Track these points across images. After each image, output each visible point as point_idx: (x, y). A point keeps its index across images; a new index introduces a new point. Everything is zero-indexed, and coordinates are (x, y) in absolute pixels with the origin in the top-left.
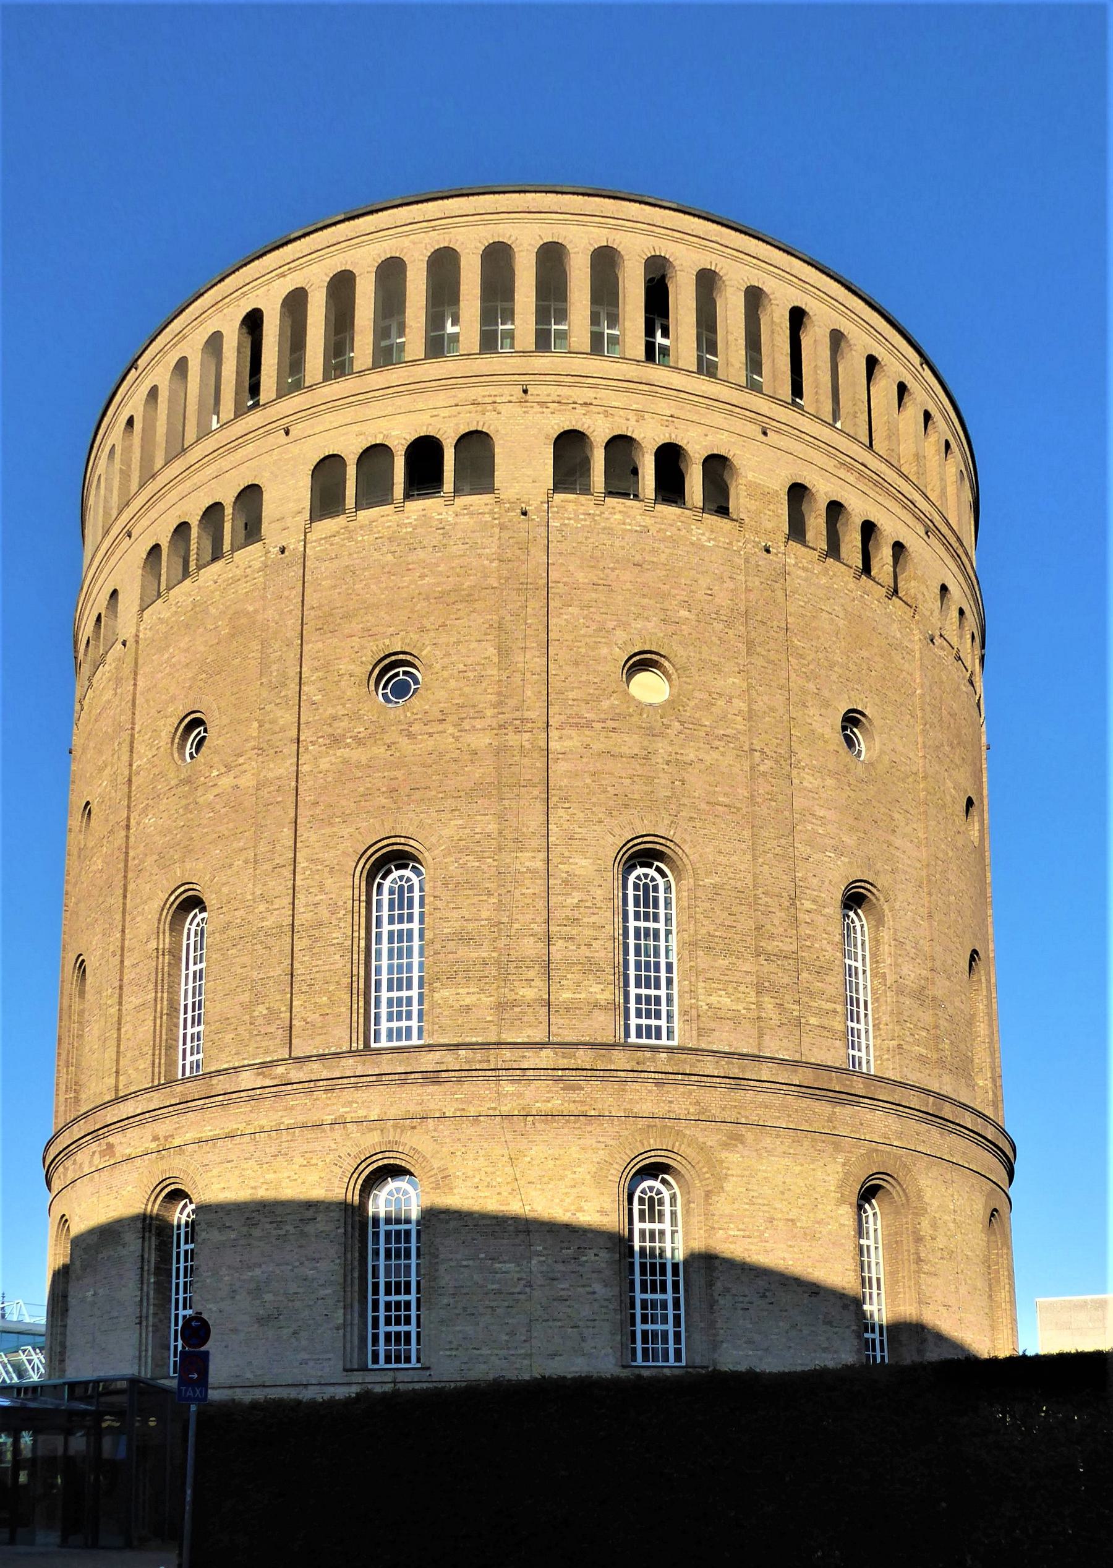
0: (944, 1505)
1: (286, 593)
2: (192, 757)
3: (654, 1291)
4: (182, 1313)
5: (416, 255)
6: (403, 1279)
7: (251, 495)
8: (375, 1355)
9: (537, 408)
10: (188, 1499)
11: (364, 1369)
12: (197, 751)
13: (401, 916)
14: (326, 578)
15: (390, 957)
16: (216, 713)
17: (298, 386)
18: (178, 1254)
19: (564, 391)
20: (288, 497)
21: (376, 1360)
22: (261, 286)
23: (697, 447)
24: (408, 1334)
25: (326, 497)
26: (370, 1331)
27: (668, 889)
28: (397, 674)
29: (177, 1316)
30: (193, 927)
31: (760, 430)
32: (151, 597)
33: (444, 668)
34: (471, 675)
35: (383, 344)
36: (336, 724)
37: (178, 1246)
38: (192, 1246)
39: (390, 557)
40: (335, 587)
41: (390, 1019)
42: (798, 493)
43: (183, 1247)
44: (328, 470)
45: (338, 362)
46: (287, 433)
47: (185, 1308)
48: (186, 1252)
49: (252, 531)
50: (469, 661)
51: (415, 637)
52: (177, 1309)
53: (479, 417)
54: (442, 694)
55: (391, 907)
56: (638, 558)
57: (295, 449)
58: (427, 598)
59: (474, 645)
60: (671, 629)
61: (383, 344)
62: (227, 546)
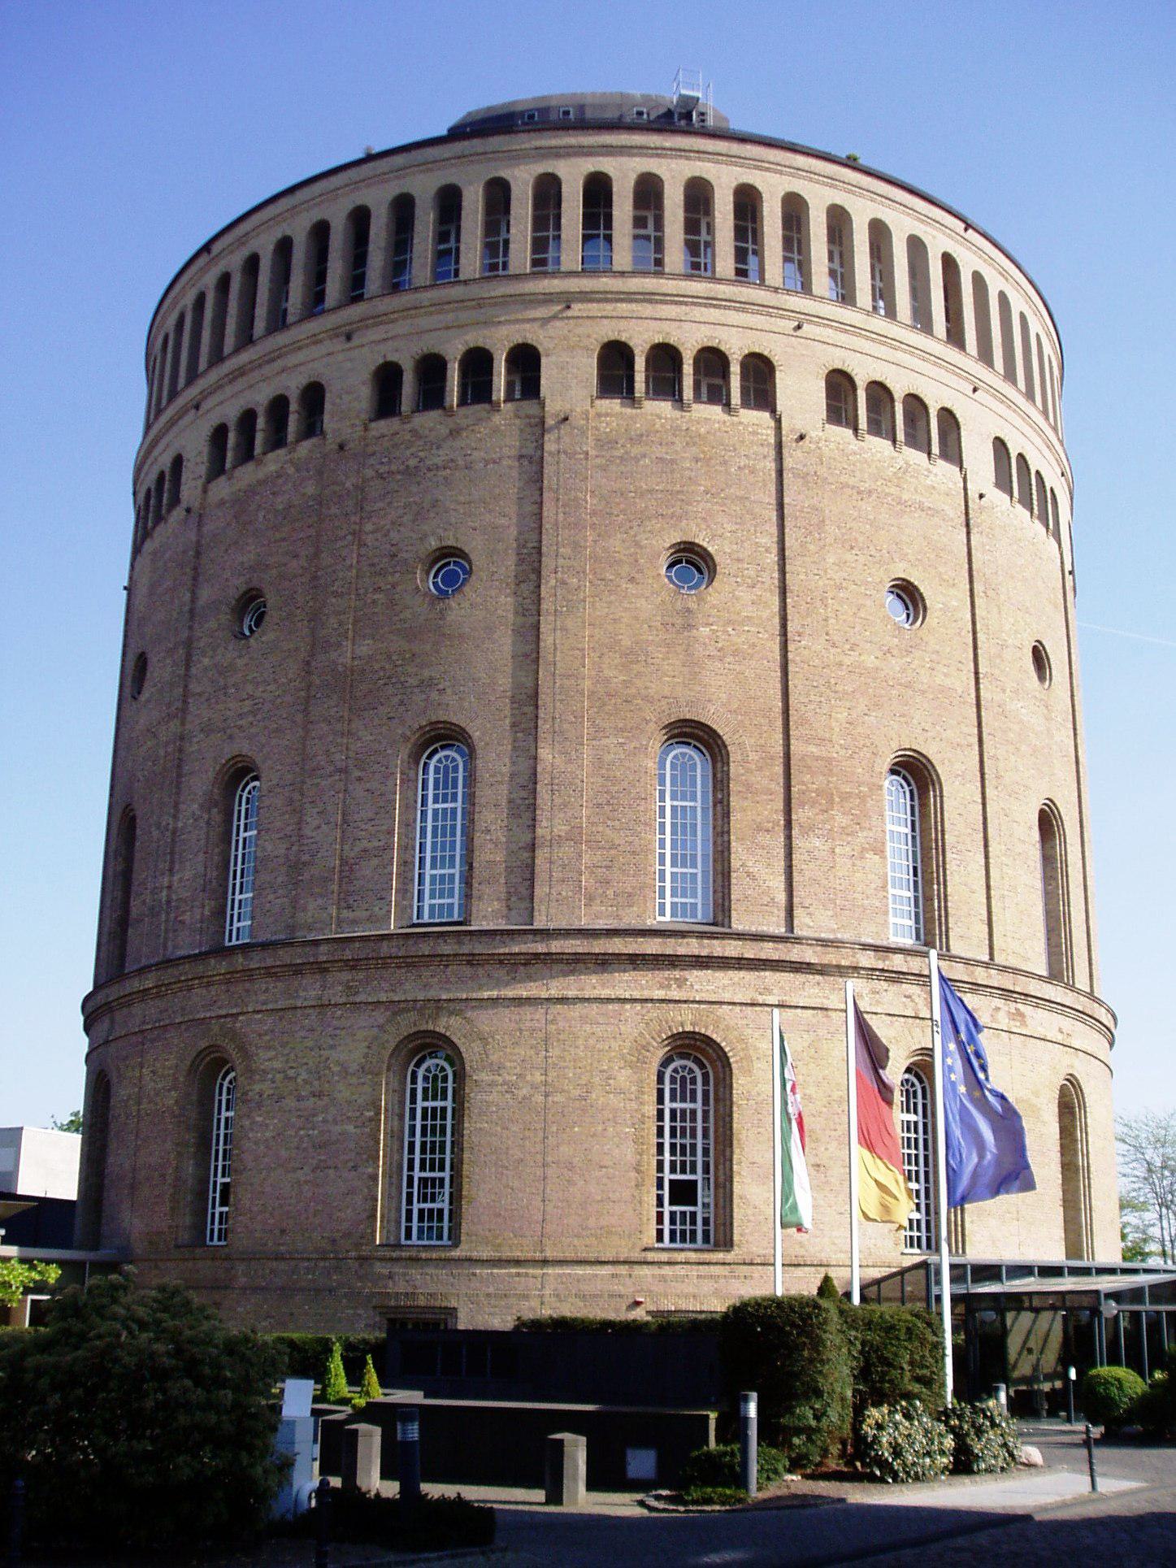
2: (251, 631)
3: (683, 1111)
4: (220, 1180)
6: (438, 1139)
7: (314, 395)
8: (409, 1230)
11: (398, 1246)
12: (257, 625)
13: (445, 796)
15: (424, 1134)
17: (359, 298)
18: (219, 1120)
20: (350, 396)
21: (409, 1236)
23: (736, 347)
24: (442, 1180)
25: (386, 401)
26: (409, 1086)
27: (705, 1076)
28: (448, 564)
29: (215, 1182)
30: (245, 795)
32: (217, 468)
35: (442, 247)
37: (219, 1113)
38: (226, 1209)
41: (432, 897)
43: (224, 1114)
44: (387, 378)
45: (397, 276)
47: (223, 1176)
48: (221, 1213)
49: (312, 426)
52: (216, 1175)
55: (436, 787)
61: (442, 247)
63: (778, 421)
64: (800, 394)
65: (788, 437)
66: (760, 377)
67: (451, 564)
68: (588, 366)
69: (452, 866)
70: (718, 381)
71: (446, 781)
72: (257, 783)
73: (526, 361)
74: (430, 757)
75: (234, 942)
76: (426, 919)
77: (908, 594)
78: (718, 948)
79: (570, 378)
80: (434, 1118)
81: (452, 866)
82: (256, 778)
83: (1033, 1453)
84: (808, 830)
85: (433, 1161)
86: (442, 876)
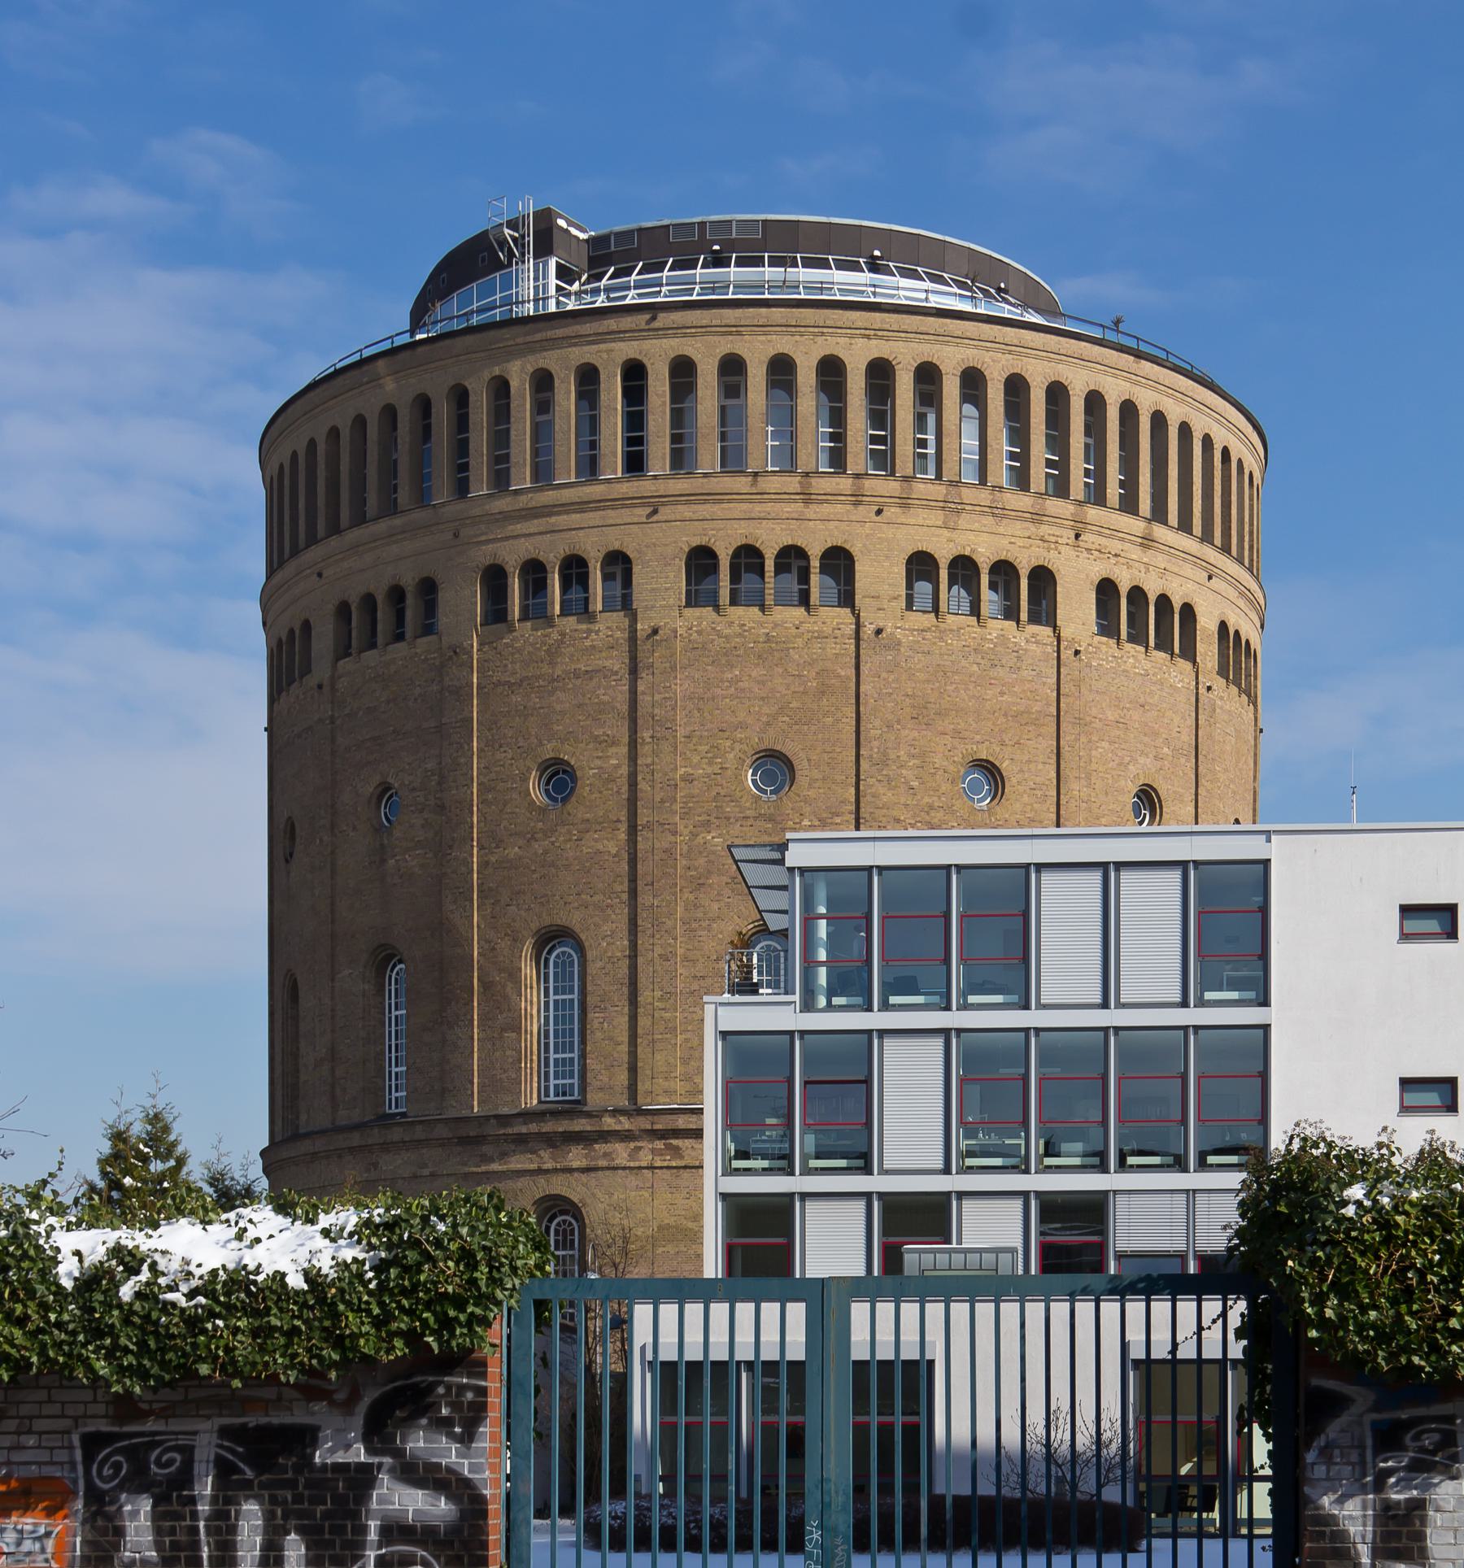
0: (1371, 1333)
1: (884, 675)
5: (996, 374)
9: (1085, 554)
10: (205, 1555)
14: (919, 670)
16: (805, 763)
19: (1103, 541)
22: (845, 335)
28: (557, 773)
31: (1206, 575)
32: (344, 650)
33: (1019, 783)
34: (1039, 793)
36: (933, 814)
39: (975, 668)
40: (928, 681)
42: (1223, 626)
46: (879, 512)
50: (1038, 780)
51: (998, 749)
53: (1045, 554)
54: (1018, 806)
56: (1142, 701)
57: (889, 532)
58: (1005, 715)
59: (1040, 766)
60: (1160, 763)
62: (380, 640)
63: (858, 618)
64: (880, 577)
65: (868, 630)
66: (839, 562)
67: (560, 778)
68: (677, 579)
69: (572, 1051)
70: (803, 563)
71: (563, 975)
72: (402, 966)
73: (619, 564)
74: (550, 952)
75: (394, 1110)
76: (552, 1098)
77: (991, 772)
78: (1111, 336)
79: (660, 585)
80: (564, 1043)
81: (572, 1051)
82: (400, 961)
83: (1436, 1481)
84: (1051, 645)
85: (564, 1009)
86: (564, 1059)
